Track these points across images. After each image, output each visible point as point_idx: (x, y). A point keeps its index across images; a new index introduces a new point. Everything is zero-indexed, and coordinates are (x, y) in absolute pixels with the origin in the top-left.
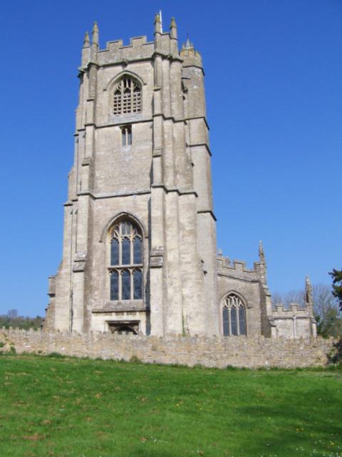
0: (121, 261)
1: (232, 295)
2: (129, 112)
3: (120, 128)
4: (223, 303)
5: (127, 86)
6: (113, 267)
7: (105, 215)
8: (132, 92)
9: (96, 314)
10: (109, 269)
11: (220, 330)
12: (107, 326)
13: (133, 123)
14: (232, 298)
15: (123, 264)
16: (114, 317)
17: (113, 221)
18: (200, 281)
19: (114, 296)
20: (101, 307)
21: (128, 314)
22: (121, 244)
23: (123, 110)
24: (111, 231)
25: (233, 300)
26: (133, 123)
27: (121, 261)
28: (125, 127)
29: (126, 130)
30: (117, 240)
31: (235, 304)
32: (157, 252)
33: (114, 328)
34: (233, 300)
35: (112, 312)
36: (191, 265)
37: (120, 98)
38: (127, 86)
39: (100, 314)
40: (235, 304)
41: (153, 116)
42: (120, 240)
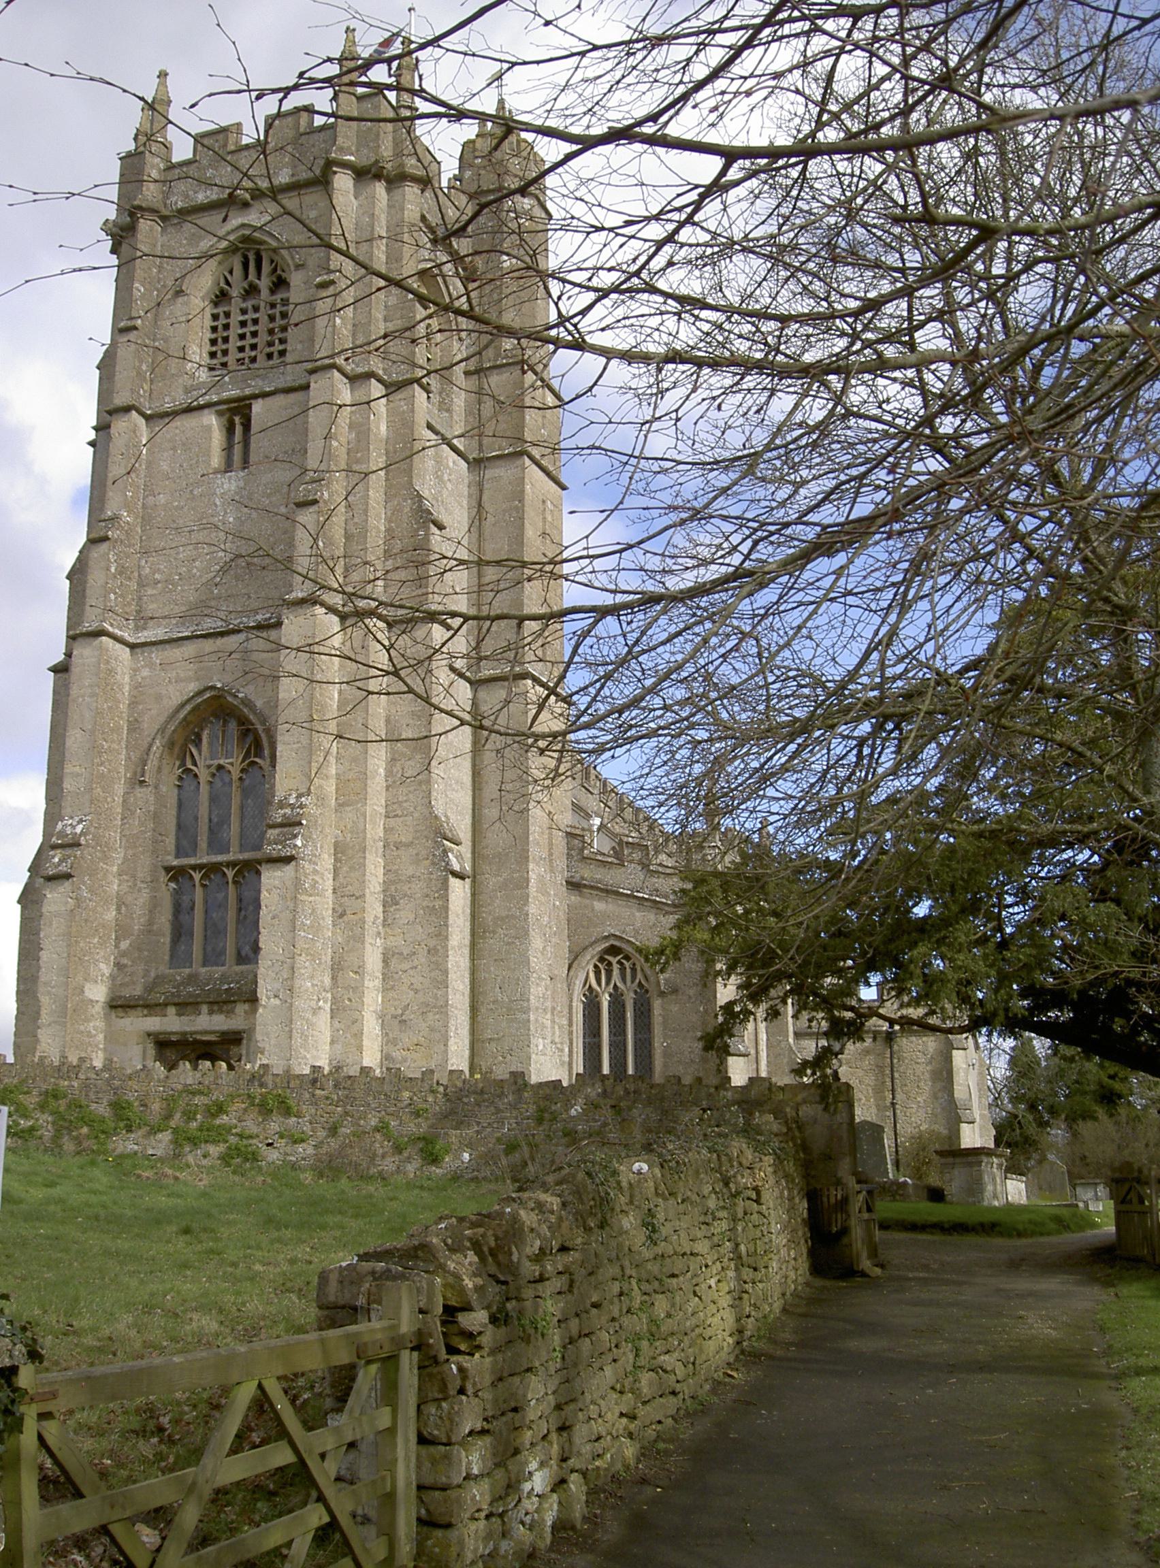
0: (203, 844)
1: (614, 950)
2: (253, 360)
3: (220, 414)
4: (587, 968)
5: (252, 276)
6: (246, 856)
7: (159, 698)
8: (265, 293)
9: (120, 1012)
10: (168, 869)
11: (206, 1032)
12: (151, 1051)
13: (255, 397)
14: (614, 960)
15: (242, 848)
16: (172, 1023)
17: (181, 715)
18: (438, 904)
19: (178, 956)
20: (138, 991)
21: (211, 1013)
22: (204, 789)
23: (233, 356)
24: (176, 750)
25: (616, 967)
26: (255, 397)
27: (203, 844)
28: (233, 411)
29: (237, 419)
30: (196, 776)
31: (599, 984)
32: (288, 811)
33: (171, 1054)
34: (616, 967)
35: (166, 1005)
36: (412, 851)
37: (227, 315)
38: (252, 276)
39: (132, 1012)
40: (599, 984)
41: (306, 387)
42: (204, 775)
